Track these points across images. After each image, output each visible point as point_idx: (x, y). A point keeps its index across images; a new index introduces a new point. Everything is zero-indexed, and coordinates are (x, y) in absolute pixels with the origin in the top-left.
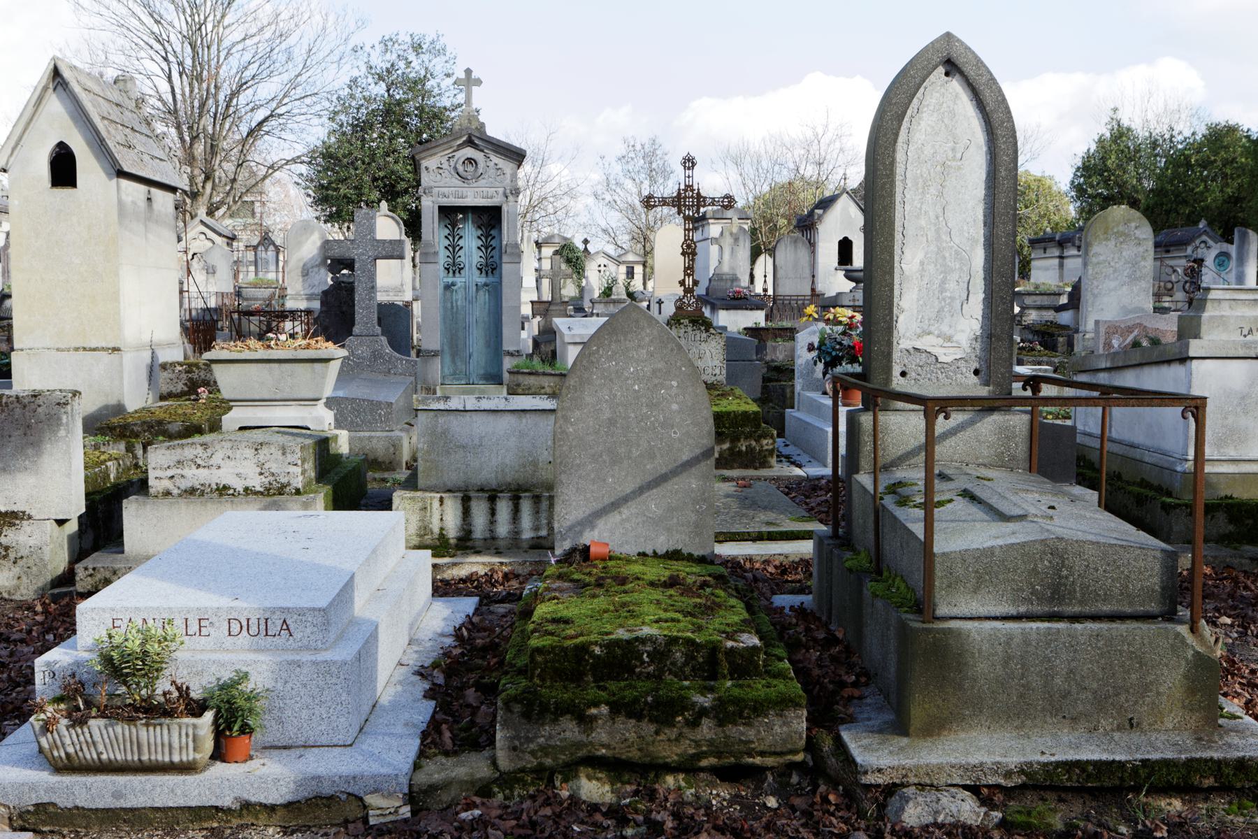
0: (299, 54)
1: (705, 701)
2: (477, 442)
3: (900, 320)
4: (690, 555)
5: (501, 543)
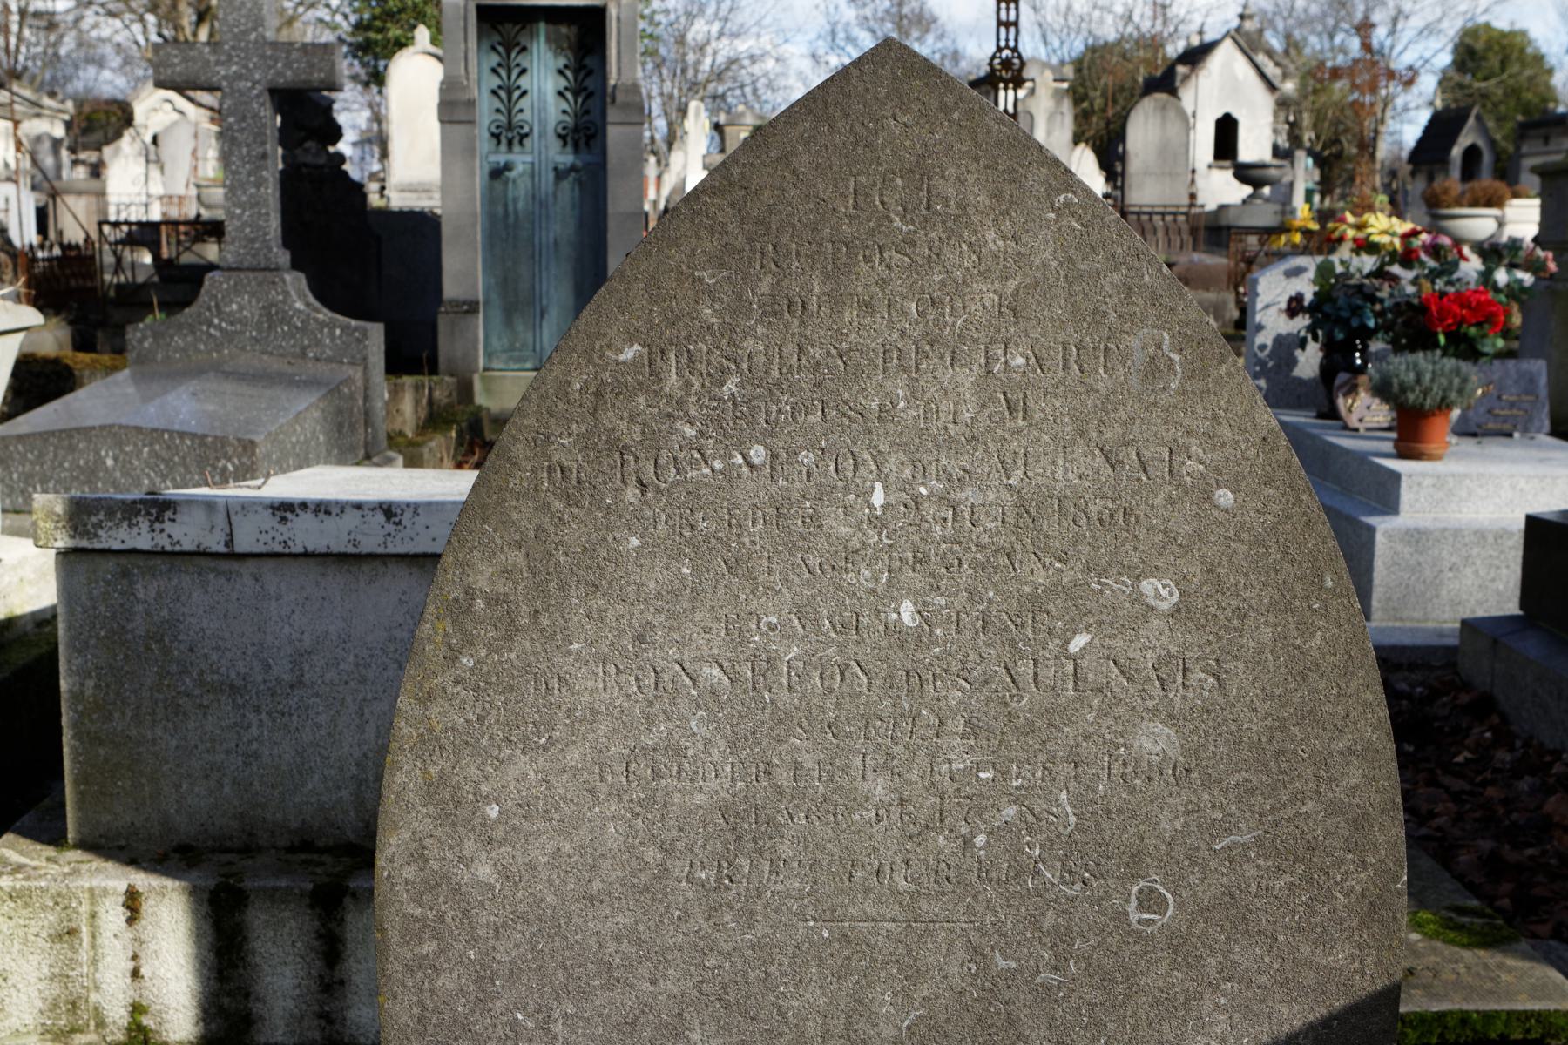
2: (282, 669)
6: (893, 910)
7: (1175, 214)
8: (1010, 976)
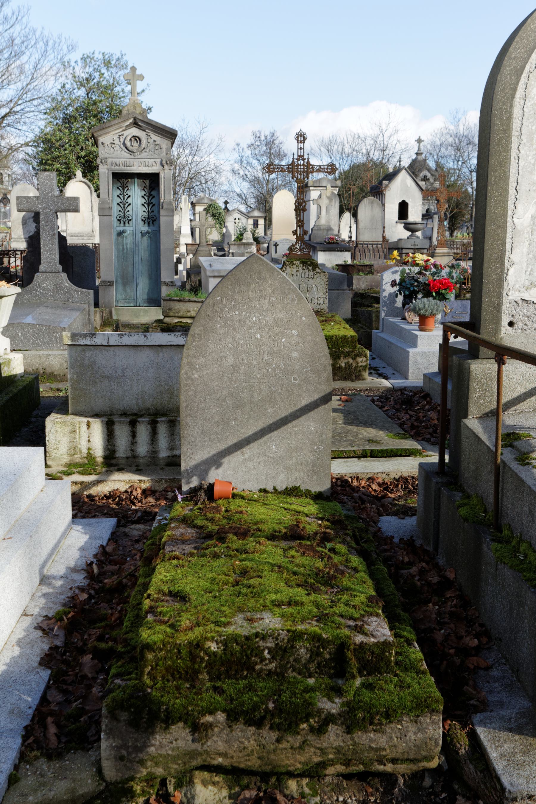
0: (29, 68)
1: (331, 706)
3: (511, 272)
4: (308, 492)
5: (141, 461)
6: (257, 381)
7: (377, 244)
8: (275, 391)
